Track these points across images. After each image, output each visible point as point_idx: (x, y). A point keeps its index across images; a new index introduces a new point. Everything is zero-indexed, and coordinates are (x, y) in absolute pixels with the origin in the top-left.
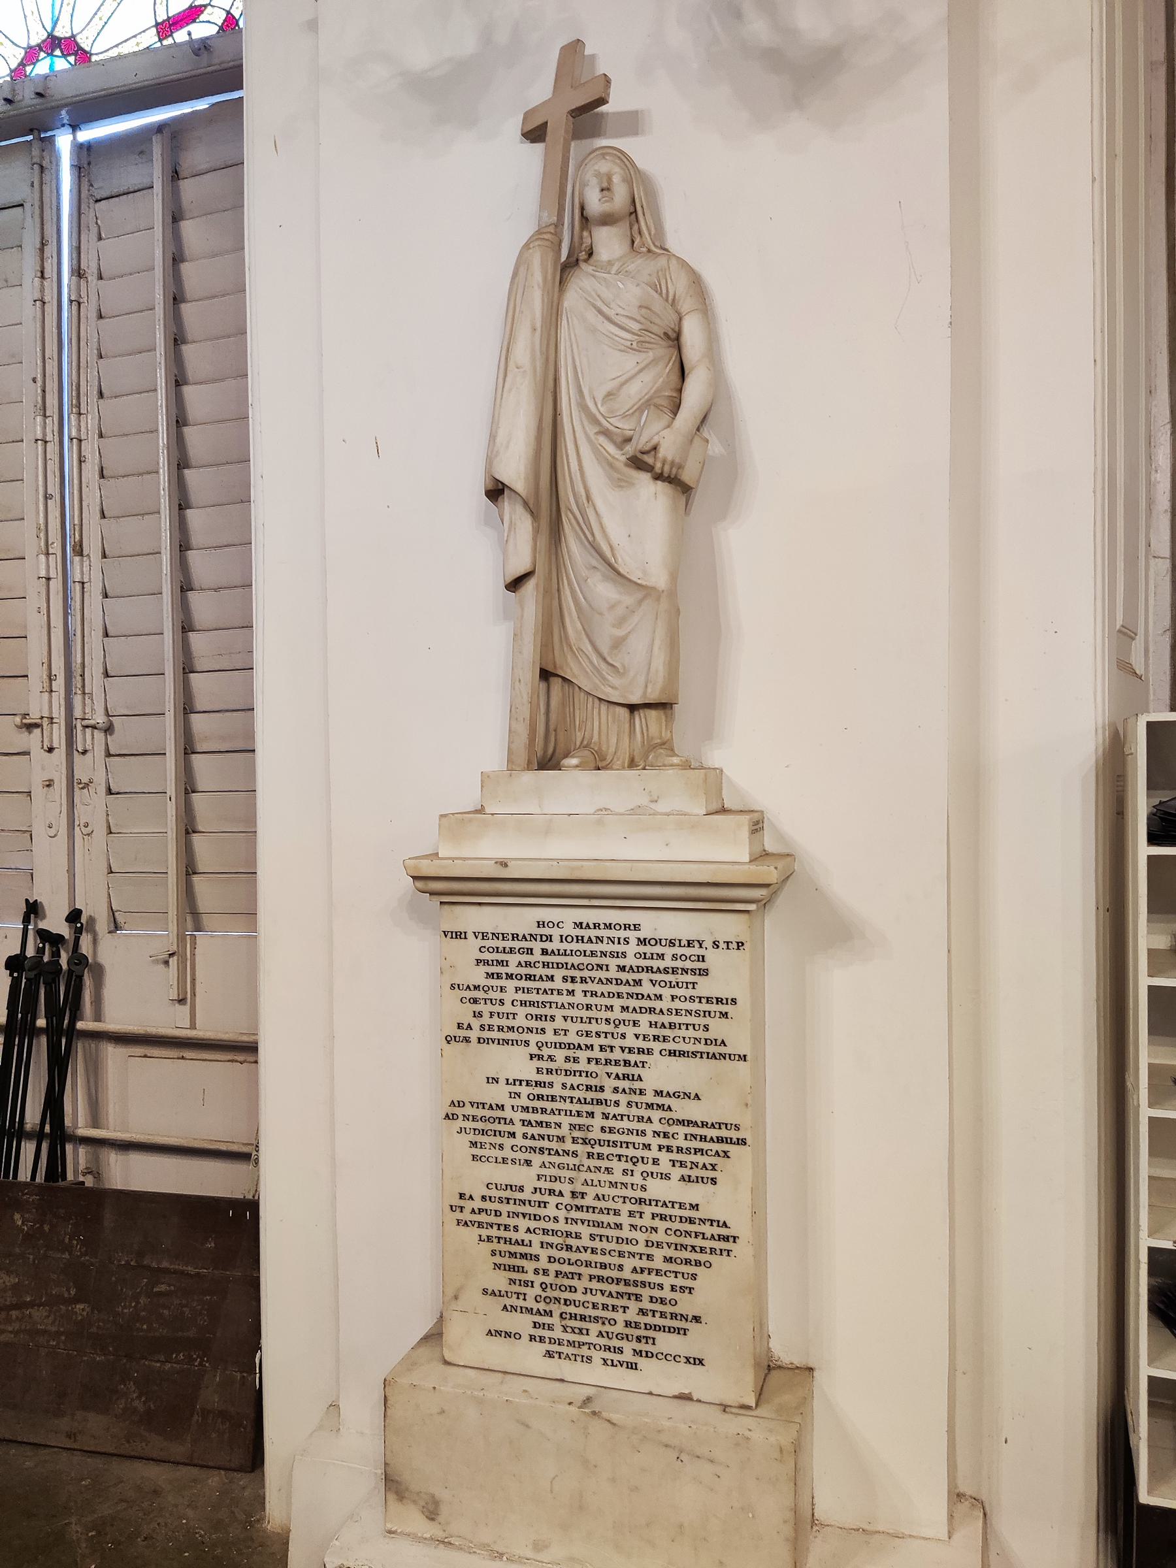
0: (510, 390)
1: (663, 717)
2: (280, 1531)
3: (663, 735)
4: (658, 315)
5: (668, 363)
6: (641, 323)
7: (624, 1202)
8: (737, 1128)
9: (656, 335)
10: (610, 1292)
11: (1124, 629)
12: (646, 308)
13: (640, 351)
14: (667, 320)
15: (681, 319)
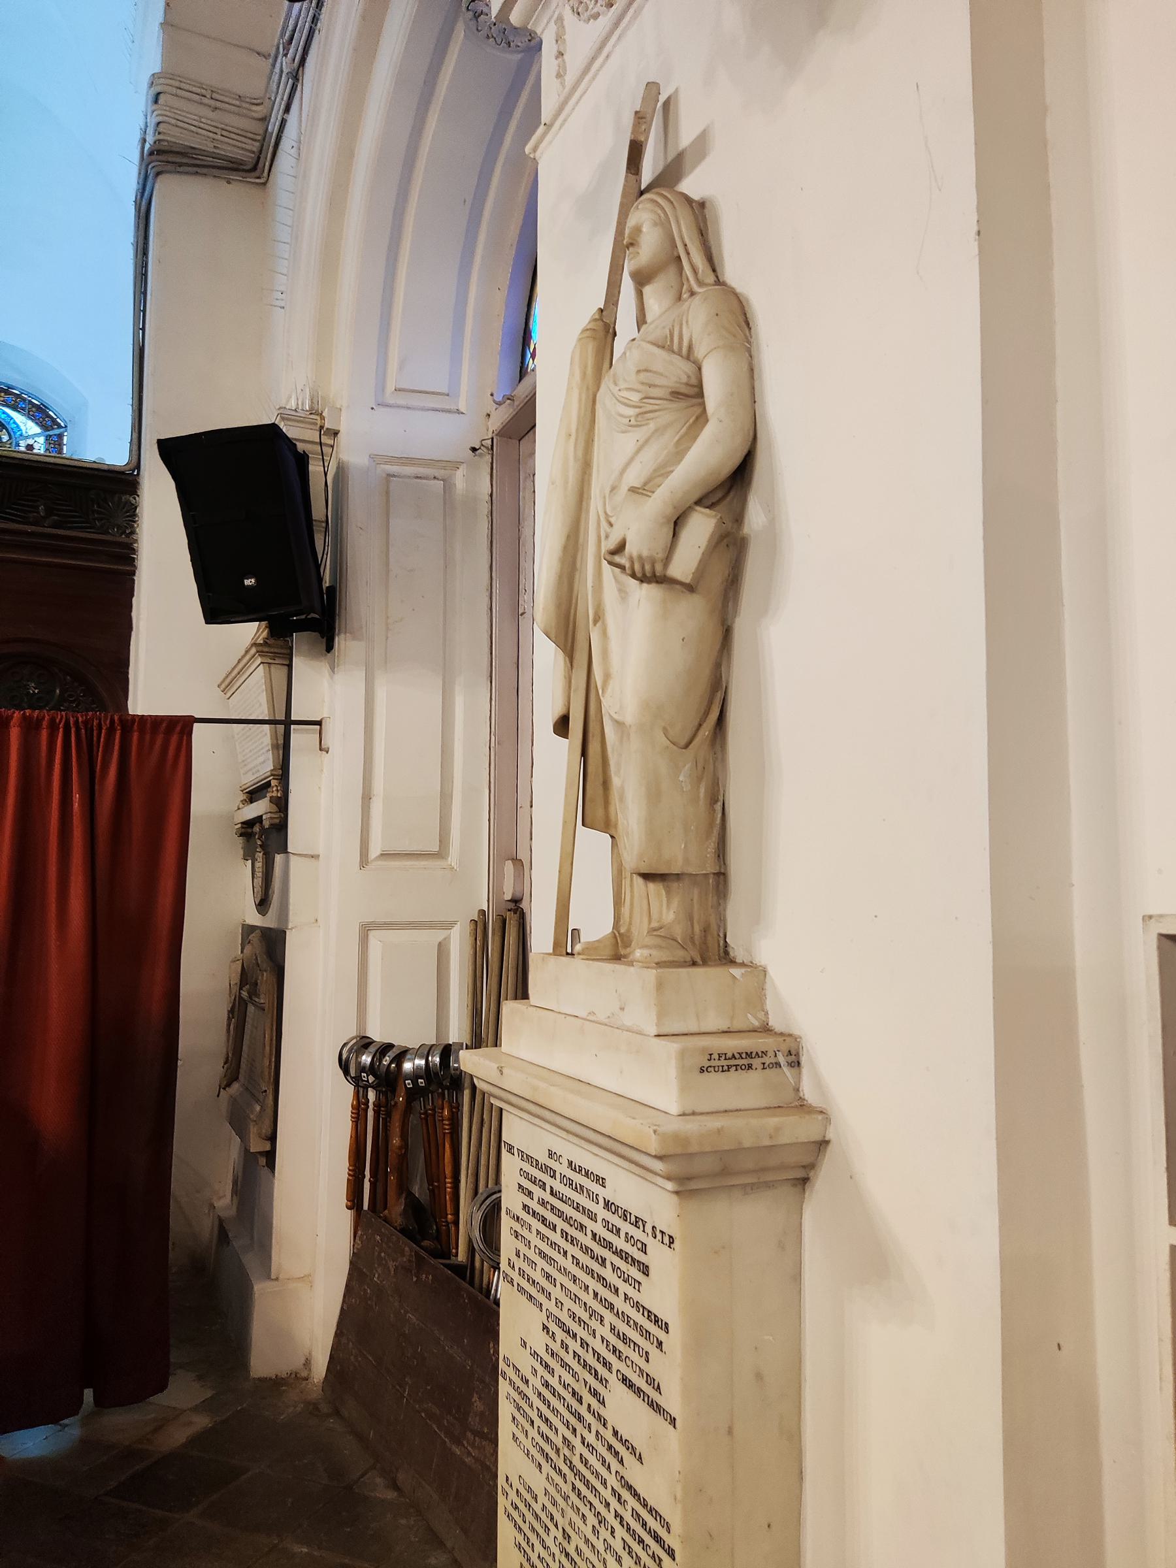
0: (524, 488)
1: (664, 892)
2: (202, 1430)
3: (664, 917)
4: (662, 375)
5: (683, 427)
6: (639, 392)
7: (736, 1070)
8: (545, 1328)
9: (660, 399)
10: (757, 1053)
11: (223, 686)
12: (646, 370)
13: (641, 426)
14: (675, 371)
15: (700, 369)
